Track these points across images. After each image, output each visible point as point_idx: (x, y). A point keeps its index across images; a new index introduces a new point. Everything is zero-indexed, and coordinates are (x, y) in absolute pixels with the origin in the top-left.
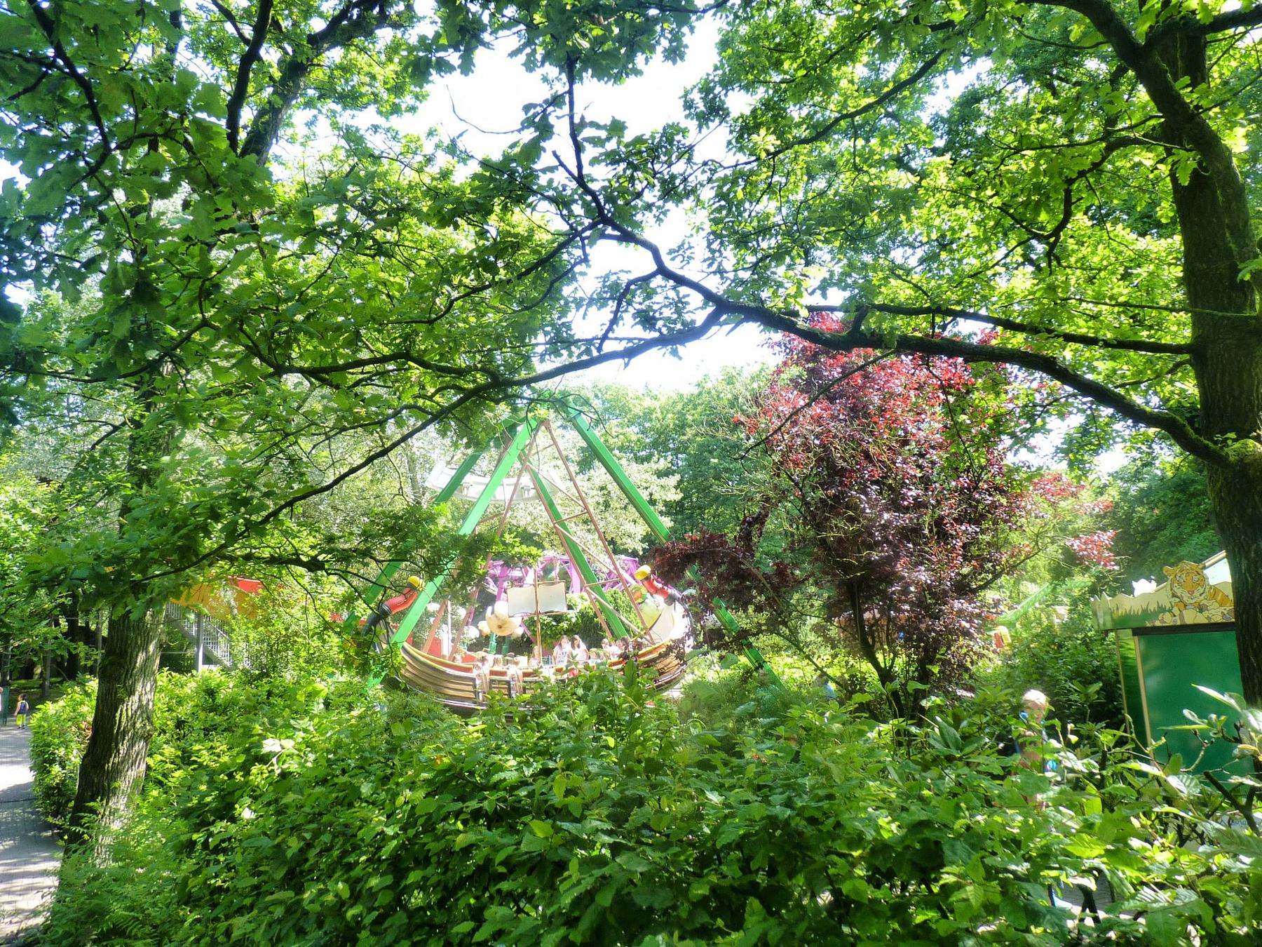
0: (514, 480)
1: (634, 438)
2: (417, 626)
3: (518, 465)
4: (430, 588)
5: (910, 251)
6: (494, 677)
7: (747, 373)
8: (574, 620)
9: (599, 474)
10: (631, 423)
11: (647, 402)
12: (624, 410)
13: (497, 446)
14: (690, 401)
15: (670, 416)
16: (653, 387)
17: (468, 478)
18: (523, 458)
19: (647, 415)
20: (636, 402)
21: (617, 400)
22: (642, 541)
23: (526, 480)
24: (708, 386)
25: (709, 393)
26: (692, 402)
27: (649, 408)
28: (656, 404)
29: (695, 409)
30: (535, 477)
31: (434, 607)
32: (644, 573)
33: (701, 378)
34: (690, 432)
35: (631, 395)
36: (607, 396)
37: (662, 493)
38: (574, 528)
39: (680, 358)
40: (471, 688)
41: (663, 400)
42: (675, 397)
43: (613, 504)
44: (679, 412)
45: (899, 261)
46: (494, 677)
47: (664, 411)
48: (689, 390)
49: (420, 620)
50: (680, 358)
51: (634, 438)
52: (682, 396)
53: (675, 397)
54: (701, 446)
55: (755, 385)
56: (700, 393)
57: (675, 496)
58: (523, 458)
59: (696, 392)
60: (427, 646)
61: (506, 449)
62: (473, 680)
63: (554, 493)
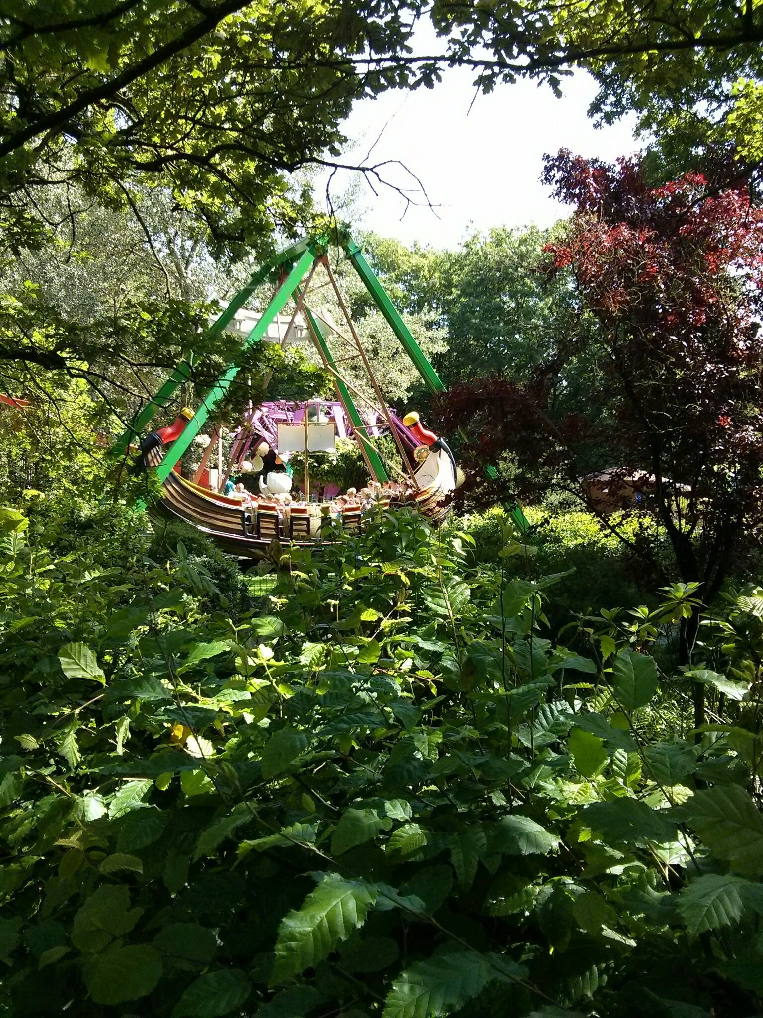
0: (289, 319)
1: (400, 294)
2: (184, 455)
3: (292, 304)
4: (198, 417)
5: (715, 105)
6: (294, 515)
7: (516, 235)
8: (335, 463)
9: (374, 320)
10: (398, 279)
11: (416, 260)
12: (393, 267)
13: (272, 282)
14: (457, 261)
15: (437, 275)
16: (422, 245)
17: (241, 314)
18: (297, 295)
19: (416, 272)
20: (406, 259)
21: (388, 256)
22: (408, 390)
23: (300, 319)
24: (477, 247)
25: (477, 254)
26: (459, 262)
27: (417, 266)
28: (425, 262)
29: (462, 269)
30: (308, 313)
31: (204, 440)
32: (412, 419)
33: (469, 239)
34: (455, 292)
35: (400, 252)
36: (378, 251)
37: (430, 345)
38: (343, 373)
39: (559, 94)
40: (239, 521)
41: (432, 258)
42: (442, 255)
43: (382, 353)
44: (446, 272)
45: (702, 114)
46: (294, 515)
47: (432, 270)
48: (458, 250)
49: (188, 450)
50: (559, 94)
51: (400, 294)
52: (450, 255)
53: (442, 255)
54: (464, 306)
55: (523, 248)
56: (468, 254)
57: (441, 348)
58: (297, 295)
59: (465, 251)
60: (196, 477)
61: (280, 284)
62: (242, 513)
63: (327, 334)
